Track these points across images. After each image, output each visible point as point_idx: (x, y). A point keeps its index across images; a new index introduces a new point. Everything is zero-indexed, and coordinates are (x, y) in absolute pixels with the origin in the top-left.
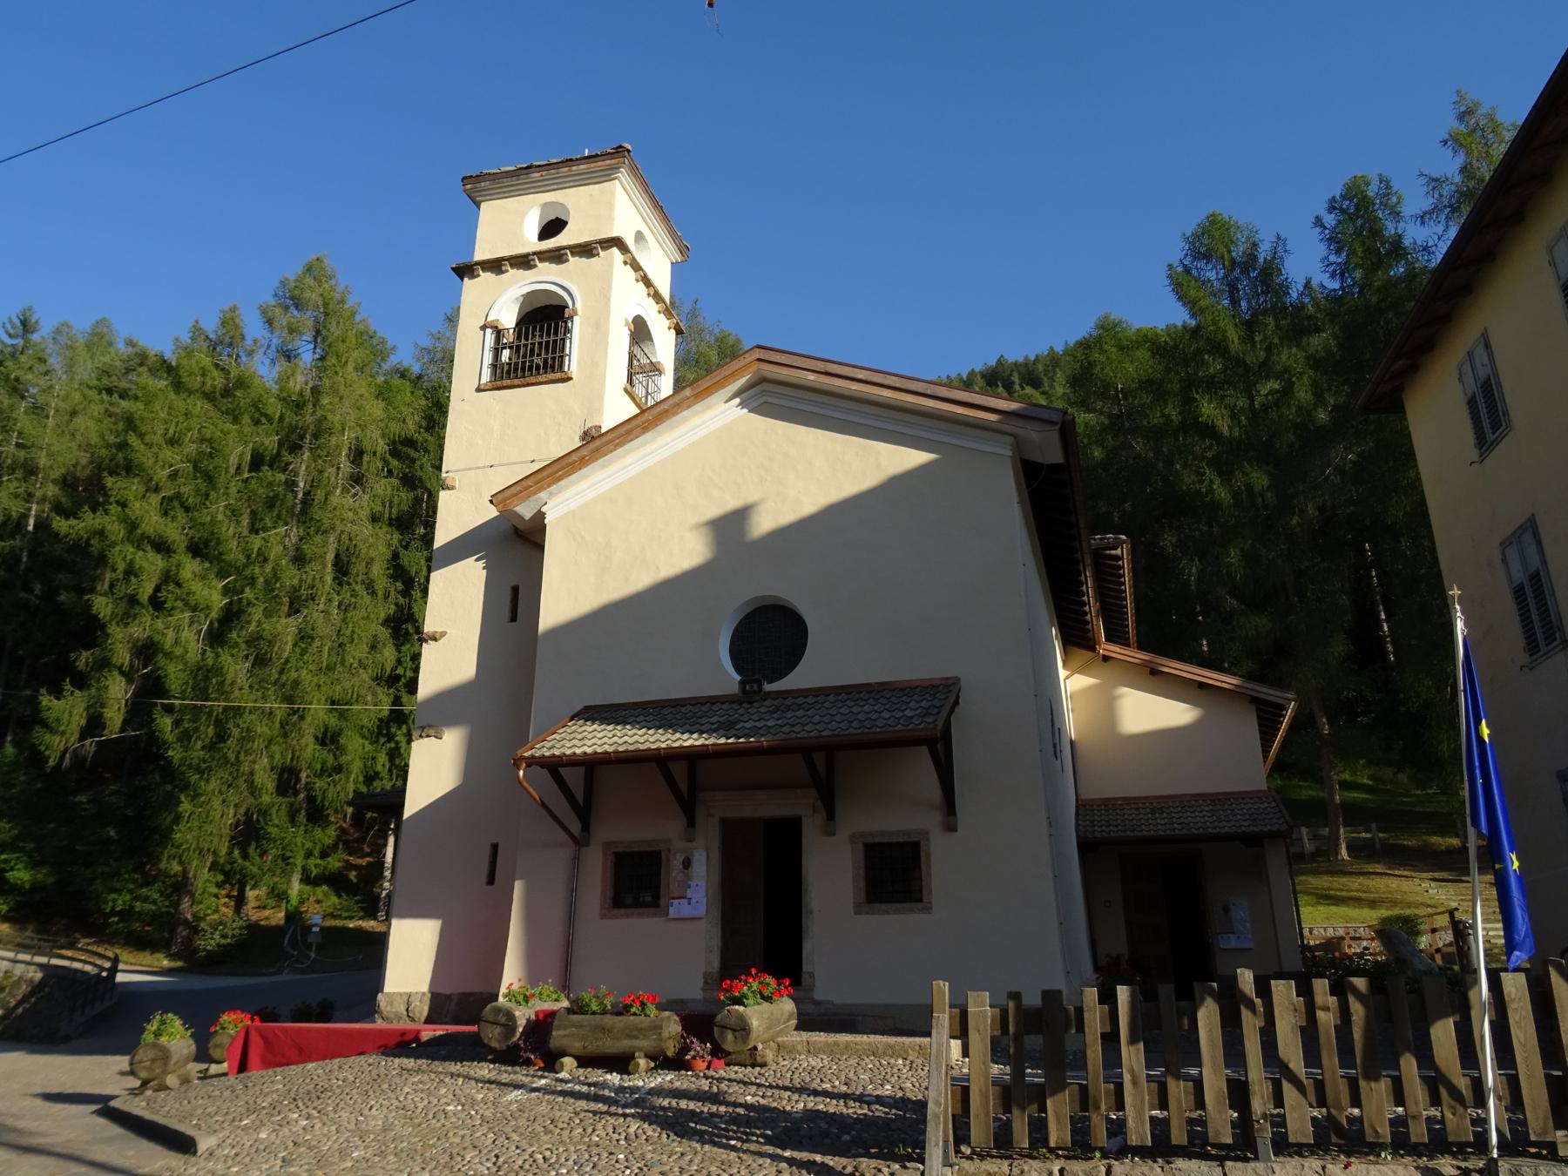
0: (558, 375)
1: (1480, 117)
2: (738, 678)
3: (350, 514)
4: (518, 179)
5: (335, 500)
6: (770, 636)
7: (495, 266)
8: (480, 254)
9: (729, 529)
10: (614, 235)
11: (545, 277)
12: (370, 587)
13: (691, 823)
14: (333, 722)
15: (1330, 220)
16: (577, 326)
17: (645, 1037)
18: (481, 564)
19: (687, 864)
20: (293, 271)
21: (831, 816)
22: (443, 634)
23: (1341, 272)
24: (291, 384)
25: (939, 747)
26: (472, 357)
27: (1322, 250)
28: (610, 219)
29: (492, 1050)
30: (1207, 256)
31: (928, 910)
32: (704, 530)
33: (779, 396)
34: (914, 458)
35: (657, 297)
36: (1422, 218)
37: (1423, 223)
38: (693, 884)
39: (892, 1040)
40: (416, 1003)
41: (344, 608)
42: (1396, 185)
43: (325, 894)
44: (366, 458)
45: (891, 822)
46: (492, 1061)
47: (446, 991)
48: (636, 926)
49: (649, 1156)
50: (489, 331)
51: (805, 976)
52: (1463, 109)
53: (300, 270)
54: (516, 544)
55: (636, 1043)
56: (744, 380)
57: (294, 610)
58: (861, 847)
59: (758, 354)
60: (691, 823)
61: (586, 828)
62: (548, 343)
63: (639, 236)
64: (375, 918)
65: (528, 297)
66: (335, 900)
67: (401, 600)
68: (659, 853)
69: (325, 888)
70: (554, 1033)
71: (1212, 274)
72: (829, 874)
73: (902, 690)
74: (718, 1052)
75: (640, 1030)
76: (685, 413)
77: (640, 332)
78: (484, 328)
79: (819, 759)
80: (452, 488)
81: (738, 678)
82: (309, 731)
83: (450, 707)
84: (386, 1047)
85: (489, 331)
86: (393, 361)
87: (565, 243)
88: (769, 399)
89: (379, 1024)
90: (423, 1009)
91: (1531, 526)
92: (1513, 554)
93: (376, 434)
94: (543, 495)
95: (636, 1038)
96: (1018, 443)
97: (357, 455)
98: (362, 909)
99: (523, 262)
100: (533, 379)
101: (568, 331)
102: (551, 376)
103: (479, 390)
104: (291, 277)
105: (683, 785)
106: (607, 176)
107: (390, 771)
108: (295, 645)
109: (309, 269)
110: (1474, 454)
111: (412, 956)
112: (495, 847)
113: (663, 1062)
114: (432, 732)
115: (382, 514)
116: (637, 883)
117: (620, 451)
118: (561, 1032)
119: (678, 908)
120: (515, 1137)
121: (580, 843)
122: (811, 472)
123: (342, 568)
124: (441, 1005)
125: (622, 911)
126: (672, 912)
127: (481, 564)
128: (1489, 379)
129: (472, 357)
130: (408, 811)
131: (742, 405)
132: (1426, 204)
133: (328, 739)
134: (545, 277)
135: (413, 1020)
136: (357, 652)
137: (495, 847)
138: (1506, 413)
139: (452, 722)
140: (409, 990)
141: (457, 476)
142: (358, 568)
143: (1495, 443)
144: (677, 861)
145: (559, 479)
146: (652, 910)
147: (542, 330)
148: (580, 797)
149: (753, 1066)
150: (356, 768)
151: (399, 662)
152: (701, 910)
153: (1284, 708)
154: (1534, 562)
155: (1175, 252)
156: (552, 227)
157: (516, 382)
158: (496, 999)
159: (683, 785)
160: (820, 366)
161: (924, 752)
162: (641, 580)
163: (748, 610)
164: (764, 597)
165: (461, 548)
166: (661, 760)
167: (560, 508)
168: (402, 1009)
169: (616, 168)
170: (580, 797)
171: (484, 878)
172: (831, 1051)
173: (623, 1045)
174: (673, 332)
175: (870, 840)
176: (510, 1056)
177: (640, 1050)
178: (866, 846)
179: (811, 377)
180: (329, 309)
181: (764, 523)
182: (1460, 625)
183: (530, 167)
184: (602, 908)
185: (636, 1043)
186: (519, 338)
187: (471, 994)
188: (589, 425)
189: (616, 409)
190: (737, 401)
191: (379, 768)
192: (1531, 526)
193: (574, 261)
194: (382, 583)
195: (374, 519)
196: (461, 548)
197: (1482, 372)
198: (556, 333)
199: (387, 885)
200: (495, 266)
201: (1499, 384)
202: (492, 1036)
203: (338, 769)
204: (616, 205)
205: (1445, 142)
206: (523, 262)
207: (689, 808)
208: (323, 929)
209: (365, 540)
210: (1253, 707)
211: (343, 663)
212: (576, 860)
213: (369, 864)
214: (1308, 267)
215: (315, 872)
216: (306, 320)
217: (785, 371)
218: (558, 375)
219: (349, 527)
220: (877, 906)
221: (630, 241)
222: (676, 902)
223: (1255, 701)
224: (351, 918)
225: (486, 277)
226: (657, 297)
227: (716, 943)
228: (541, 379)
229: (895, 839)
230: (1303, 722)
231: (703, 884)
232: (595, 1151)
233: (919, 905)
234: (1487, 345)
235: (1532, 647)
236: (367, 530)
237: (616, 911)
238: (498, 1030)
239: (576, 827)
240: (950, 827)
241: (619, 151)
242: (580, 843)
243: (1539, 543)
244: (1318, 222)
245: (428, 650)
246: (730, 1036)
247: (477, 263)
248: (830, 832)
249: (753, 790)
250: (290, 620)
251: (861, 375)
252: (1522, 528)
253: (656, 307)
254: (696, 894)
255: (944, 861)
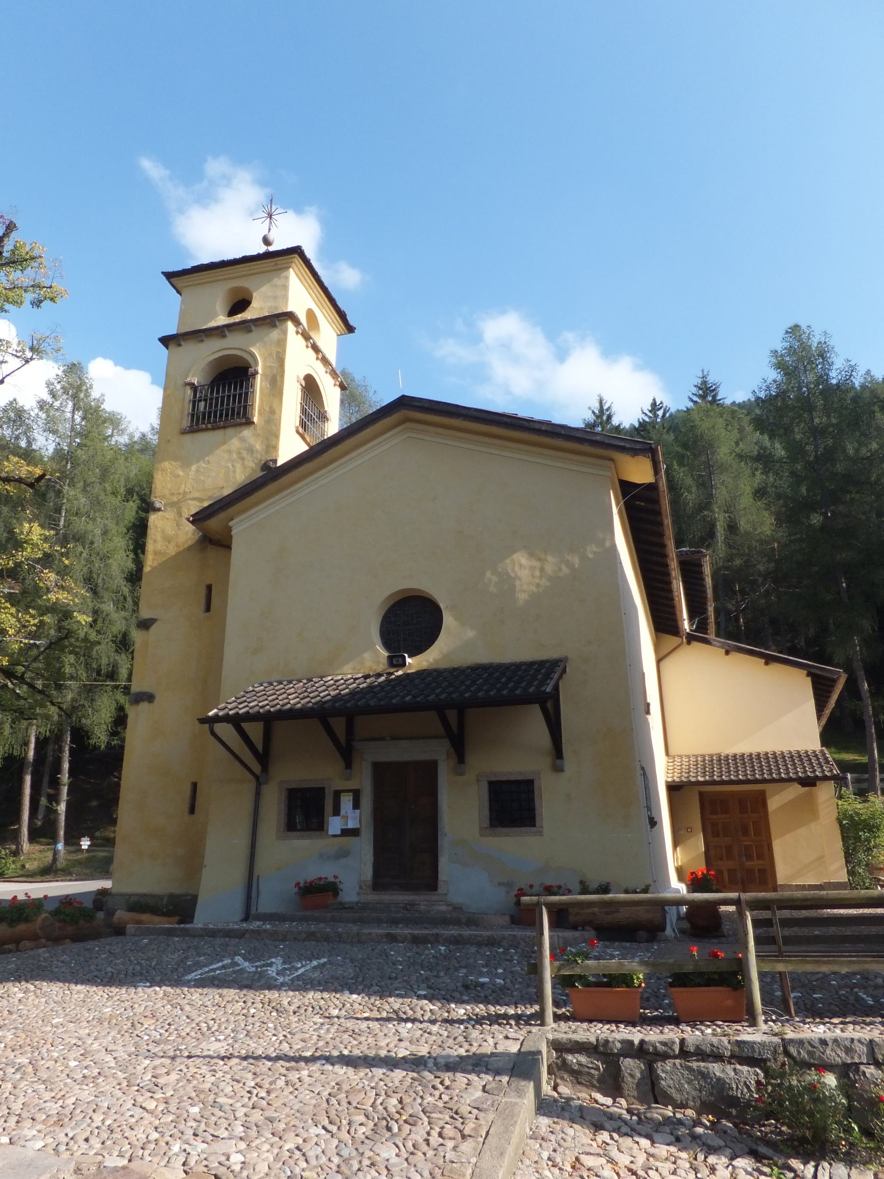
2: (386, 654)
10: (289, 310)
11: (232, 344)
16: (259, 382)
25: (549, 705)
28: (286, 298)
35: (325, 361)
45: (510, 765)
49: (294, 1025)
58: (485, 786)
63: (310, 314)
72: (460, 810)
77: (310, 388)
79: (452, 715)
81: (386, 654)
105: (341, 735)
116: (306, 811)
120: (187, 1008)
121: (259, 781)
125: (294, 834)
134: (232, 344)
146: (318, 833)
148: (260, 747)
153: (834, 681)
158: (664, 929)
159: (341, 735)
161: (536, 708)
163: (392, 603)
164: (403, 591)
170: (260, 747)
171: (186, 807)
174: (338, 390)
175: (494, 779)
178: (491, 784)
182: (873, 730)
189: (290, 446)
207: (347, 755)
212: (258, 794)
218: (244, 421)
221: (303, 319)
226: (325, 361)
230: (852, 688)
232: (250, 1020)
239: (257, 768)
240: (558, 769)
242: (259, 781)
253: (332, 381)
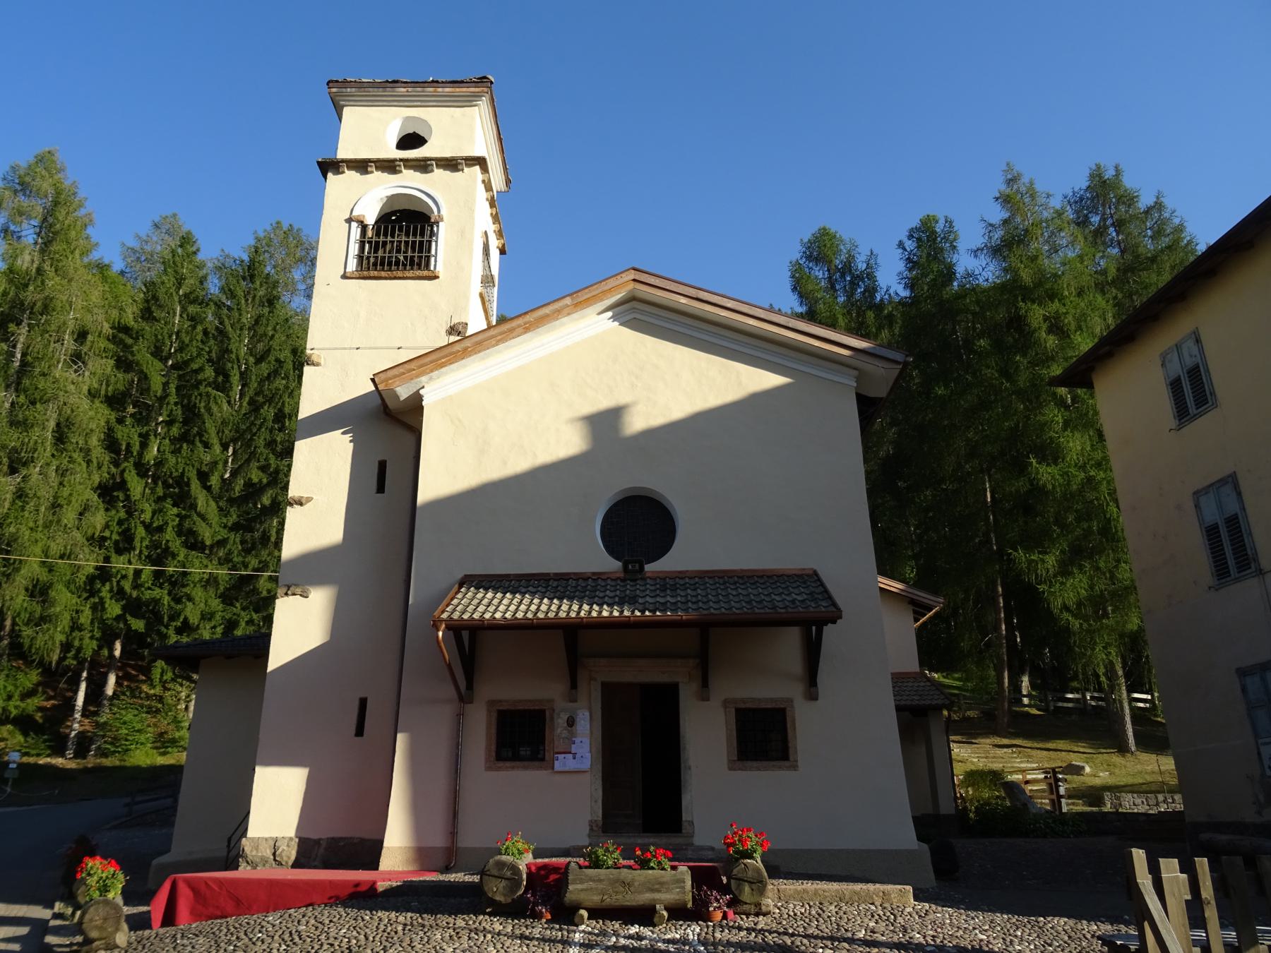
0: (425, 273)
1: (1022, 185)
3: (72, 387)
4: (384, 90)
5: (58, 372)
6: (638, 524)
7: (362, 166)
8: (342, 154)
9: (604, 424)
11: (409, 183)
12: (86, 452)
13: (574, 685)
14: (44, 576)
15: (910, 245)
17: (668, 890)
18: (348, 437)
19: (571, 722)
20: (24, 159)
21: (705, 684)
22: (309, 500)
23: (912, 285)
24: (19, 262)
26: (336, 246)
27: (901, 266)
29: (492, 902)
30: (817, 260)
31: (794, 767)
32: (579, 425)
33: (642, 313)
34: (770, 380)
36: (975, 253)
37: (976, 256)
38: (577, 740)
39: (858, 887)
40: (282, 847)
41: (62, 472)
42: (957, 226)
43: (10, 732)
44: (90, 338)
45: (761, 690)
46: (490, 914)
47: (314, 836)
48: (522, 780)
50: (354, 225)
51: (685, 825)
52: (1009, 177)
53: (32, 160)
54: (390, 423)
55: (657, 896)
56: (619, 296)
57: (13, 471)
59: (632, 275)
60: (574, 685)
61: (470, 686)
62: (414, 242)
64: (63, 755)
65: (392, 198)
66: (21, 738)
67: (113, 470)
68: (543, 712)
69: (10, 727)
70: (570, 887)
71: (819, 273)
72: (705, 735)
73: (742, 577)
74: (734, 903)
75: (662, 884)
76: (565, 320)
78: (349, 221)
80: (318, 365)
82: (22, 579)
83: (316, 568)
84: (337, 898)
85: (354, 225)
86: (95, 256)
87: (428, 155)
88: (638, 316)
89: (244, 871)
90: (291, 853)
91: (1231, 481)
92: (1209, 504)
93: (101, 318)
94: (424, 379)
95: (659, 891)
96: (861, 377)
97: (81, 336)
98: (49, 747)
99: (389, 166)
100: (400, 274)
101: (432, 234)
102: (419, 273)
103: (344, 277)
104: (24, 165)
106: (468, 101)
107: (92, 622)
108: (13, 503)
109: (40, 160)
110: (1173, 423)
111: (277, 803)
112: (363, 703)
113: (679, 913)
114: (298, 590)
115: (98, 391)
116: (522, 738)
117: (501, 346)
118: (579, 887)
119: (563, 762)
121: (465, 697)
122: (679, 384)
123: (60, 437)
124: (311, 851)
126: (558, 766)
127: (348, 437)
128: (1197, 366)
129: (336, 246)
130: (274, 663)
131: (614, 318)
132: (979, 241)
133: (39, 591)
134: (409, 183)
135: (280, 864)
136: (69, 516)
137: (363, 703)
138: (1213, 394)
139: (319, 581)
140: (274, 835)
141: (323, 354)
142: (75, 439)
143: (1195, 417)
144: (561, 721)
145: (442, 366)
147: (400, 230)
149: (757, 915)
150: (65, 622)
151: (107, 526)
152: (586, 764)
154: (1232, 507)
155: (795, 252)
156: (411, 140)
157: (383, 274)
160: (692, 292)
162: (519, 464)
164: (635, 488)
165: (326, 421)
166: (571, 630)
167: (437, 392)
168: (269, 854)
169: (478, 96)
172: (801, 897)
173: (644, 898)
176: (516, 910)
177: (660, 902)
178: (738, 710)
179: (683, 300)
180: (59, 201)
181: (637, 423)
183: (394, 82)
184: (487, 760)
185: (657, 896)
186: (378, 235)
187: (341, 839)
188: (455, 321)
190: (610, 314)
191: (82, 620)
192: (1231, 481)
193: (438, 173)
194: (98, 452)
195: (92, 395)
196: (326, 421)
197: (1189, 362)
198: (422, 235)
199: (76, 726)
200: (362, 166)
201: (1207, 371)
202: (497, 890)
203: (44, 619)
204: (463, 128)
205: (997, 199)
206: (389, 166)
208: (21, 766)
209: (85, 413)
210: (911, 607)
211: (59, 521)
212: (460, 716)
213: (54, 706)
214: (891, 280)
215: (14, 712)
216: (37, 207)
217: (660, 293)
218: (425, 273)
219: (72, 400)
220: (749, 763)
222: (561, 757)
223: (913, 602)
224: (38, 755)
225: (350, 175)
227: (599, 794)
228: (407, 274)
229: (763, 706)
231: (587, 741)
233: (787, 763)
234: (1198, 341)
235: (1221, 572)
236: (85, 404)
237: (501, 764)
238: (504, 883)
240: (812, 695)
241: (483, 80)
243: (1239, 494)
244: (901, 245)
245: (292, 514)
246: (747, 888)
247: (343, 161)
248: (705, 697)
249: (611, 659)
250: (9, 479)
251: (730, 304)
252: (1222, 482)
254: (580, 749)
255: (808, 725)
